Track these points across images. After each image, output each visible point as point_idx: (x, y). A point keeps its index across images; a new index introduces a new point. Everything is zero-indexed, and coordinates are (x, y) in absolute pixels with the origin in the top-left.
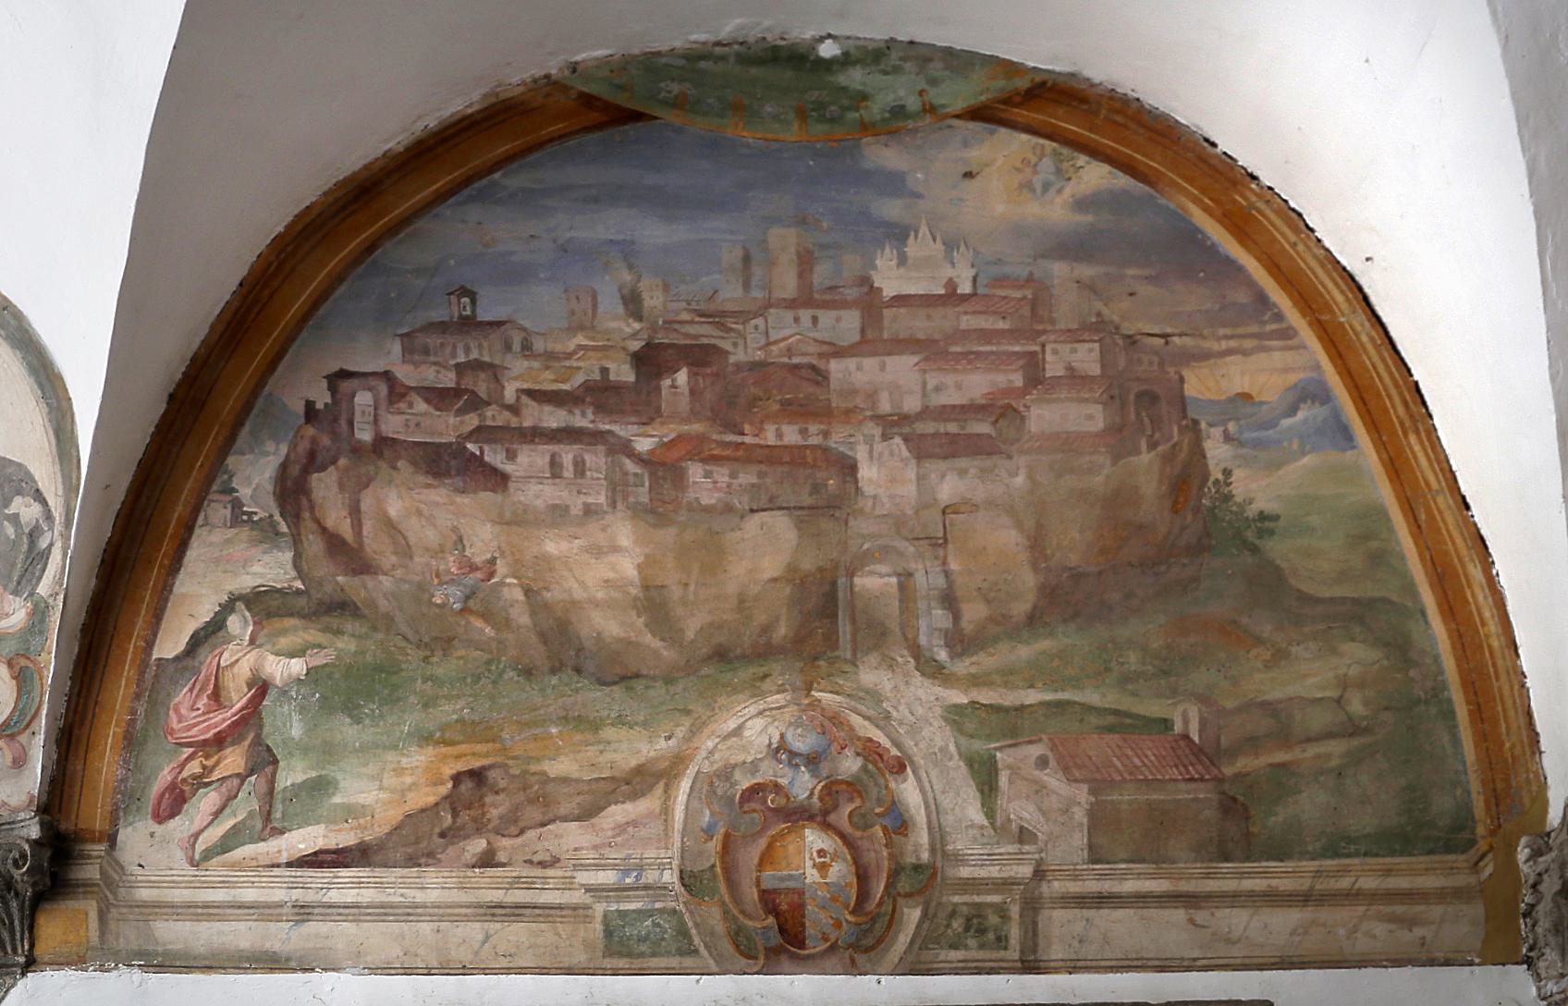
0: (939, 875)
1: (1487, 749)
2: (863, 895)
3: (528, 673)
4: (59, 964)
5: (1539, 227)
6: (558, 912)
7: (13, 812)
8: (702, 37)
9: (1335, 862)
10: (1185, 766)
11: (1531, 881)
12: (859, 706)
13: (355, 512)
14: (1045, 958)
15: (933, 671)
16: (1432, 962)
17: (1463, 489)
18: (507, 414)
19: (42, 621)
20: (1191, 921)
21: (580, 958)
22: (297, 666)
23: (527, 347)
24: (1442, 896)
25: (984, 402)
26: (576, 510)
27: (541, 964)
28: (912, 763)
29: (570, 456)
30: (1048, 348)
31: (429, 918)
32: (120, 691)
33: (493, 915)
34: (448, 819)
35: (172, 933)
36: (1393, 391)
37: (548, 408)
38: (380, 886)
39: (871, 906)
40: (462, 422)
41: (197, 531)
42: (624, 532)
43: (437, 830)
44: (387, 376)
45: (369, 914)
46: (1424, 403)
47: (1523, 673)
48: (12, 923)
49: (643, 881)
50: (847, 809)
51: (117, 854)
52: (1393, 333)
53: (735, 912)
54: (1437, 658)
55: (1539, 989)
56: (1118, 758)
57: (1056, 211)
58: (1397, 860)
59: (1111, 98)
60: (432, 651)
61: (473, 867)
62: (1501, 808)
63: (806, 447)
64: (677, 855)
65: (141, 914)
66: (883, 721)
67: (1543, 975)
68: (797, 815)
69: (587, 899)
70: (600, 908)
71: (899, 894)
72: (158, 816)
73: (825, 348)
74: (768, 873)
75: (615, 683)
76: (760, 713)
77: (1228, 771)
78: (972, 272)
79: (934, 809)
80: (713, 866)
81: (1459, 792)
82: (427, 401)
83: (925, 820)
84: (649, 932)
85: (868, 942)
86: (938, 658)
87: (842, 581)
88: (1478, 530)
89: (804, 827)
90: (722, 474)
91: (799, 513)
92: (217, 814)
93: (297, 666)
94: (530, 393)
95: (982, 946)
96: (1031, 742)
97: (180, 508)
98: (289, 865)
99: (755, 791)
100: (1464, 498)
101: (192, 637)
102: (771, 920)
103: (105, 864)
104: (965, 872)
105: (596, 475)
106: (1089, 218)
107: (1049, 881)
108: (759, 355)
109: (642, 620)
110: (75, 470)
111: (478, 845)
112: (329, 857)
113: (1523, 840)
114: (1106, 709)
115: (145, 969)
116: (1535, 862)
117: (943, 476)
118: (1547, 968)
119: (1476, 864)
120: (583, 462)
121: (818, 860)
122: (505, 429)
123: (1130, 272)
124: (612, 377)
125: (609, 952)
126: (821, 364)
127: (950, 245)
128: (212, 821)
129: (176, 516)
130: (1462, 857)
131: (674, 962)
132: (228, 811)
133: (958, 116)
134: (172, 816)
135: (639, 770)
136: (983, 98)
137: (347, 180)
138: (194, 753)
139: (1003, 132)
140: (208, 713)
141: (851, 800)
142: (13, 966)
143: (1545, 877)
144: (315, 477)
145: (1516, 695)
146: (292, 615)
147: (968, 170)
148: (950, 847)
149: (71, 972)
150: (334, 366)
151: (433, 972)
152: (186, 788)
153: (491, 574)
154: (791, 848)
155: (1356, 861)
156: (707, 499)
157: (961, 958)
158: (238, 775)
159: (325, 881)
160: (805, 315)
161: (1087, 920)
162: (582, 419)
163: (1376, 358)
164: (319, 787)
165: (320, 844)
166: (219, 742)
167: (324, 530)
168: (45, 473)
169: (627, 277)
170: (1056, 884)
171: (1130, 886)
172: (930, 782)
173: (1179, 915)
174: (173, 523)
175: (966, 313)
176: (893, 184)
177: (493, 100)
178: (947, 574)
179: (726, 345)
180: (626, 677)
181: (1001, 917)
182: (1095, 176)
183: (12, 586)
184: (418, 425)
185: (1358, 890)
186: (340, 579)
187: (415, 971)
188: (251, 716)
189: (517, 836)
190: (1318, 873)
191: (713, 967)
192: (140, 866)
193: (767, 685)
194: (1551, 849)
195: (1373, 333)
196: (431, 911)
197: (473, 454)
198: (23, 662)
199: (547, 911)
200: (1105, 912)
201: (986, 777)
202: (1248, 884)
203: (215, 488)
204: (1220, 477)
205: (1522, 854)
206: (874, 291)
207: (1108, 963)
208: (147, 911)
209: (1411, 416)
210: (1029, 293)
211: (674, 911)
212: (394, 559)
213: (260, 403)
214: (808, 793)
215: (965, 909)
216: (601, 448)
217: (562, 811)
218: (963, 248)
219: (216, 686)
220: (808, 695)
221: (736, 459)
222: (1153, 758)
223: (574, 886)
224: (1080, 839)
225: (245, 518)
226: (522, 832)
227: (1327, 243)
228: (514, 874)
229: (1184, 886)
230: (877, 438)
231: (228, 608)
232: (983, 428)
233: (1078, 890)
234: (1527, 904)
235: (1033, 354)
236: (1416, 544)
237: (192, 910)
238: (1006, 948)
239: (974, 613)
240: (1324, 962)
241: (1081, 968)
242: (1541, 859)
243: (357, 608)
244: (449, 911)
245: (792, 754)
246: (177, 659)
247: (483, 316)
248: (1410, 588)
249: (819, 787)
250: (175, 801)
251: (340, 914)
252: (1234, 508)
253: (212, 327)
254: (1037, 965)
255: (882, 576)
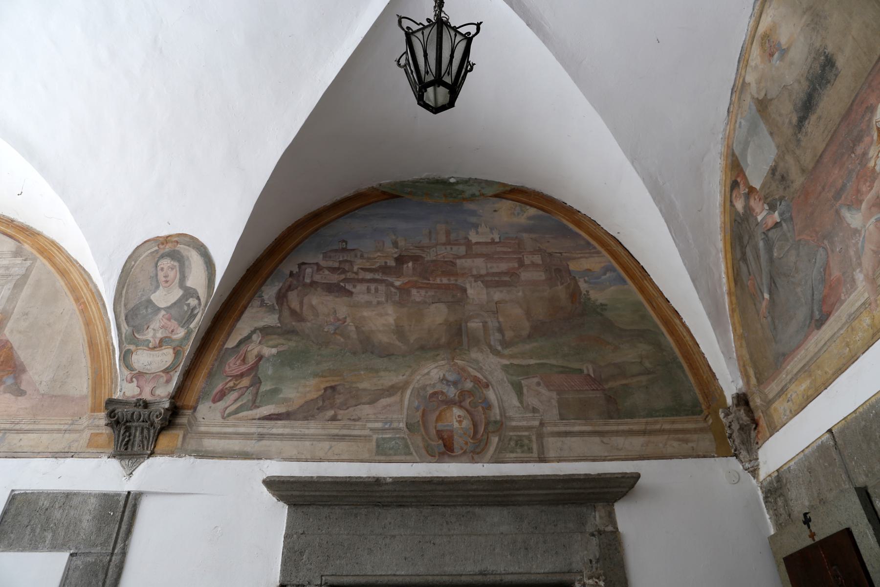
0: (504, 425)
1: (698, 378)
2: (476, 432)
3: (355, 353)
4: (163, 454)
5: (668, 225)
6: (360, 438)
7: (161, 398)
8: (417, 177)
9: (652, 419)
10: (590, 385)
11: (728, 425)
12: (471, 365)
13: (301, 303)
14: (548, 456)
15: (497, 353)
16: (698, 456)
17: (666, 296)
18: (354, 275)
19: (189, 336)
20: (602, 442)
21: (366, 456)
22: (274, 351)
23: (362, 256)
24: (695, 431)
25: (505, 271)
26: (375, 302)
27: (351, 458)
28: (491, 385)
29: (374, 287)
30: (525, 256)
31: (309, 440)
32: (210, 359)
33: (334, 439)
34: (320, 403)
35: (210, 444)
36: (635, 268)
37: (367, 273)
38: (292, 427)
39: (479, 436)
40: (340, 277)
41: (248, 309)
42: (390, 309)
43: (316, 407)
44: (317, 264)
45: (287, 438)
46: (646, 272)
47: (703, 353)
48: (149, 438)
49: (392, 426)
50: (468, 401)
51: (196, 414)
52: (631, 252)
53: (427, 438)
54: (671, 348)
55: (743, 466)
56: (566, 382)
57: (522, 220)
58: (675, 418)
59: (534, 192)
60: (322, 346)
61: (328, 421)
62: (709, 399)
63: (450, 284)
64: (405, 417)
65: (199, 436)
66: (480, 370)
67: (743, 461)
68: (450, 403)
69: (370, 433)
70: (375, 437)
71: (489, 432)
72: (214, 401)
73: (455, 256)
74: (439, 424)
75: (385, 357)
76: (436, 367)
77: (606, 387)
78: (499, 236)
79: (500, 401)
80: (419, 421)
81: (692, 393)
82: (329, 271)
83: (497, 405)
84: (394, 446)
85: (478, 450)
86: (498, 349)
87: (463, 325)
88: (674, 308)
89: (453, 407)
90: (423, 292)
91: (448, 303)
92: (236, 401)
93: (274, 351)
94: (362, 269)
95: (523, 452)
96: (534, 377)
97: (244, 302)
98: (259, 419)
99: (435, 394)
100: (667, 299)
101: (240, 341)
102: (441, 442)
103: (190, 417)
104: (514, 424)
105: (382, 292)
106: (532, 222)
107: (546, 427)
108: (434, 258)
109: (395, 336)
110: (212, 290)
111: (331, 413)
112: (275, 417)
113: (720, 410)
114: (559, 366)
115: (196, 457)
116: (727, 418)
117: (495, 293)
118: (744, 458)
119: (705, 419)
120: (378, 288)
121: (458, 419)
122: (353, 279)
123: (547, 236)
124: (388, 264)
125: (378, 453)
126: (454, 261)
127: (492, 229)
128: (234, 403)
129: (242, 304)
130: (699, 417)
131: (403, 458)
132: (240, 399)
133: (491, 196)
134: (219, 400)
135: (392, 387)
136: (497, 192)
137: (311, 213)
138: (232, 379)
139: (504, 200)
140: (240, 365)
141: (470, 397)
142: (145, 454)
143: (732, 423)
144: (290, 293)
145: (703, 360)
146: (274, 334)
147: (495, 209)
148: (507, 414)
149: (167, 458)
150: (301, 261)
151: (308, 460)
152: (226, 391)
153: (345, 322)
154: (448, 415)
155: (660, 418)
156: (418, 299)
157: (515, 456)
158: (246, 387)
159: (272, 425)
160: (448, 247)
161: (562, 442)
162: (378, 276)
163: (628, 259)
164: (275, 391)
165: (272, 411)
166: (242, 375)
167: (290, 308)
168: (202, 292)
169: (394, 237)
170: (549, 428)
171: (577, 428)
172: (498, 391)
173: (597, 439)
174: (241, 306)
175: (498, 247)
176: (473, 213)
177: (357, 193)
178: (499, 322)
179: (424, 255)
180: (389, 355)
181: (529, 441)
182: (532, 211)
183: (182, 325)
184: (325, 278)
185: (664, 429)
186: (293, 323)
187: (301, 460)
188: (255, 367)
189: (346, 409)
190: (647, 423)
191: (418, 460)
192: (203, 418)
193: (438, 358)
194: (731, 413)
195: (625, 252)
196: (310, 437)
197: (342, 286)
198: (179, 348)
199: (355, 438)
200: (568, 438)
201: (519, 390)
202: (621, 428)
203: (256, 296)
204: (585, 293)
205: (722, 415)
206: (469, 241)
207: (573, 458)
208: (202, 435)
209: (643, 275)
210: (517, 241)
211: (403, 438)
212: (312, 317)
213: (276, 271)
214: (454, 395)
215: (515, 437)
216: (384, 284)
217: (363, 401)
218: (495, 229)
219: (244, 357)
220: (453, 361)
221: (427, 288)
222: (578, 382)
223: (366, 428)
224: (555, 411)
225: (265, 305)
226: (348, 408)
227: (605, 229)
228: (344, 424)
229: (597, 429)
230: (473, 282)
231: (253, 332)
232: (507, 279)
233: (558, 430)
234: (729, 434)
235: (520, 258)
236: (655, 313)
237: (219, 435)
238: (532, 453)
239: (509, 334)
240: (657, 457)
241: (562, 460)
242: (729, 417)
243: (298, 332)
244: (317, 437)
245: (448, 381)
246: (233, 348)
247: (349, 247)
248: (656, 326)
249: (458, 393)
250: (222, 395)
251: (275, 438)
252: (592, 302)
253: (265, 251)
254: (545, 459)
255: (477, 323)
